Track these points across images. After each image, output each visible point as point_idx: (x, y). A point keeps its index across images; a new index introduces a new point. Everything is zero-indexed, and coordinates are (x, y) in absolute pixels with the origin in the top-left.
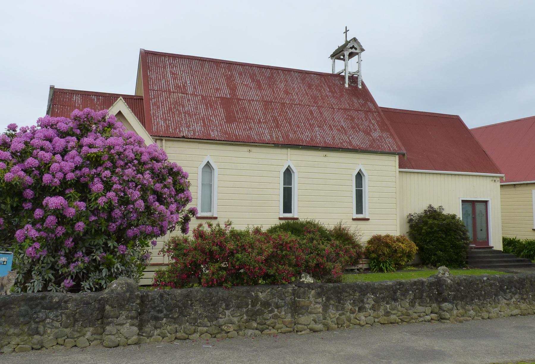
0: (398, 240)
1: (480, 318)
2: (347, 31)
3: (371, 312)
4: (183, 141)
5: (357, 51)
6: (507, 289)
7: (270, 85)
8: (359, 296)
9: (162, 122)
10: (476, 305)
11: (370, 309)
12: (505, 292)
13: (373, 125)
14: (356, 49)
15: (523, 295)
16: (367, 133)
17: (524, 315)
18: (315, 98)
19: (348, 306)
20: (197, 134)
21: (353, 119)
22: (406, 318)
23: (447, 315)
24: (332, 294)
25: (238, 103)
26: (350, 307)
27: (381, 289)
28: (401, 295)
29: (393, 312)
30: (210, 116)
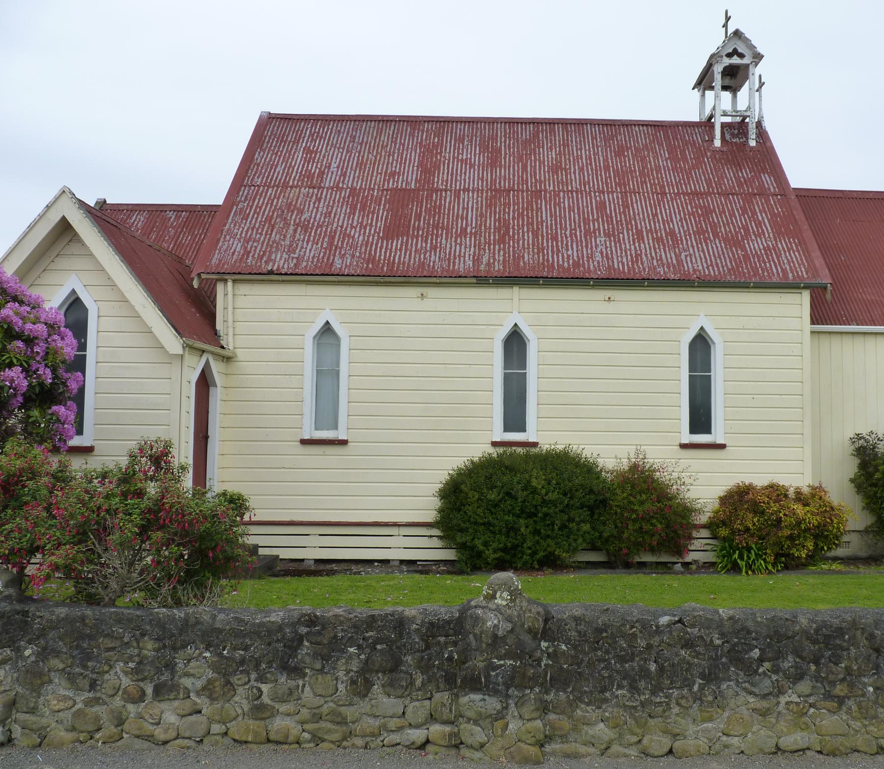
0: (800, 497)
1: (633, 752)
2: (728, 19)
3: (202, 702)
4: (272, 281)
5: (746, 61)
6: (761, 660)
7: (520, 159)
8: (157, 650)
9: (239, 245)
10: (617, 705)
11: (198, 694)
12: (750, 669)
13: (759, 224)
14: (741, 56)
15: (833, 683)
16: (733, 242)
17: (833, 753)
18: (622, 178)
19: (119, 676)
20: (305, 264)
21: (707, 212)
22: (329, 731)
23: (475, 734)
24: (61, 639)
25: (429, 196)
26: (126, 681)
27: (238, 634)
28: (315, 655)
29: (283, 708)
30: (352, 227)
